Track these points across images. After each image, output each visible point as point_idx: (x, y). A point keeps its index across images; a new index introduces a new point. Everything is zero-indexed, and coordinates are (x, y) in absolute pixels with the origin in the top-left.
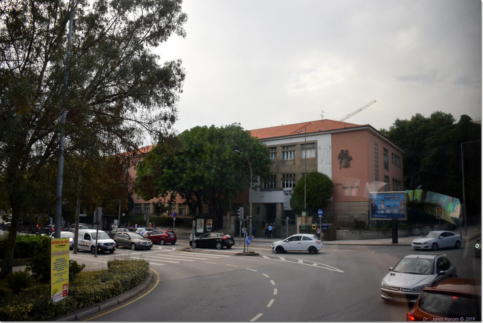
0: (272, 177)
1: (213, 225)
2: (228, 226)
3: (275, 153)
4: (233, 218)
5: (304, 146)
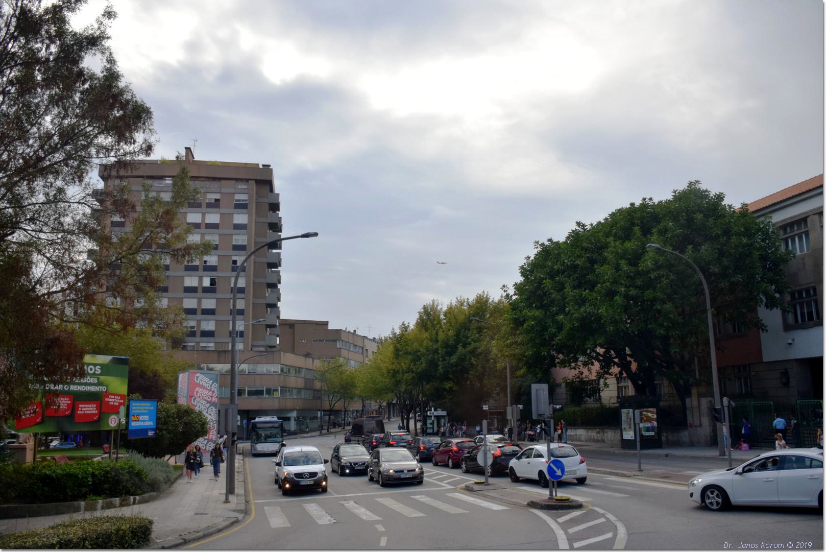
0: (808, 292)
1: (657, 420)
2: (697, 422)
3: (807, 234)
4: (704, 402)
5: (113, 486)
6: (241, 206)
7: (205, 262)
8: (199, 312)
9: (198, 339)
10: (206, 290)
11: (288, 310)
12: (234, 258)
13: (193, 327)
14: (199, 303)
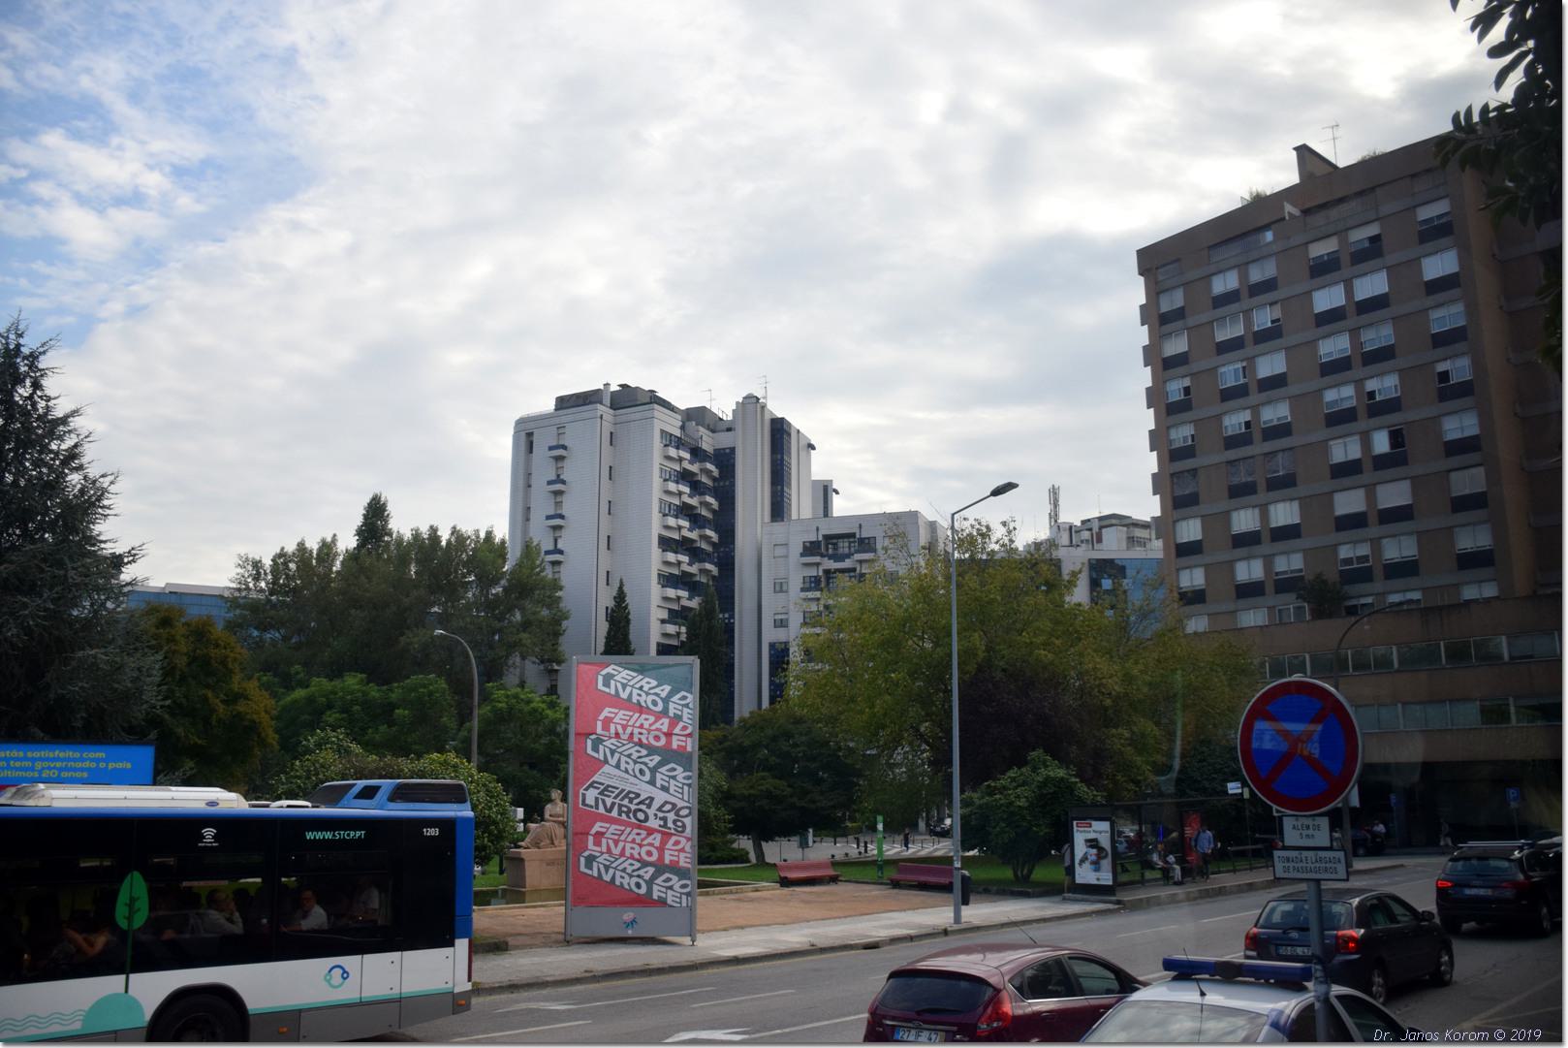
6: (1436, 233)
7: (1371, 395)
8: (1373, 518)
9: (1378, 586)
10: (1381, 462)
11: (728, 416)
12: (1441, 367)
13: (1365, 558)
14: (1371, 498)
